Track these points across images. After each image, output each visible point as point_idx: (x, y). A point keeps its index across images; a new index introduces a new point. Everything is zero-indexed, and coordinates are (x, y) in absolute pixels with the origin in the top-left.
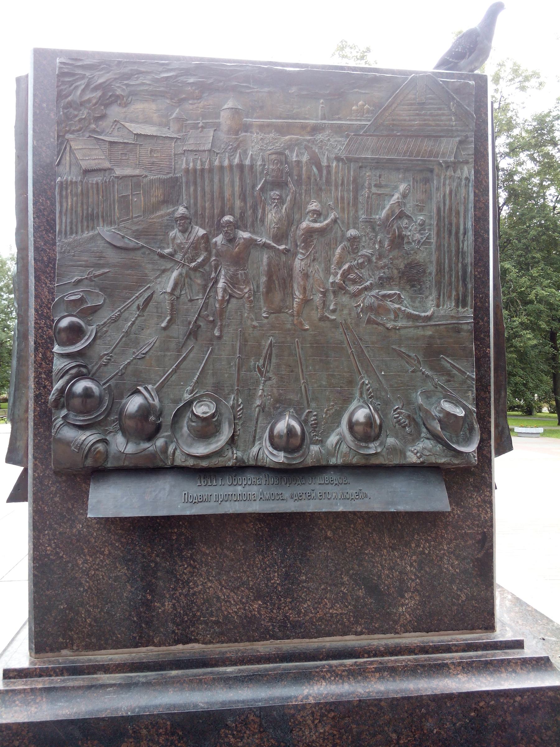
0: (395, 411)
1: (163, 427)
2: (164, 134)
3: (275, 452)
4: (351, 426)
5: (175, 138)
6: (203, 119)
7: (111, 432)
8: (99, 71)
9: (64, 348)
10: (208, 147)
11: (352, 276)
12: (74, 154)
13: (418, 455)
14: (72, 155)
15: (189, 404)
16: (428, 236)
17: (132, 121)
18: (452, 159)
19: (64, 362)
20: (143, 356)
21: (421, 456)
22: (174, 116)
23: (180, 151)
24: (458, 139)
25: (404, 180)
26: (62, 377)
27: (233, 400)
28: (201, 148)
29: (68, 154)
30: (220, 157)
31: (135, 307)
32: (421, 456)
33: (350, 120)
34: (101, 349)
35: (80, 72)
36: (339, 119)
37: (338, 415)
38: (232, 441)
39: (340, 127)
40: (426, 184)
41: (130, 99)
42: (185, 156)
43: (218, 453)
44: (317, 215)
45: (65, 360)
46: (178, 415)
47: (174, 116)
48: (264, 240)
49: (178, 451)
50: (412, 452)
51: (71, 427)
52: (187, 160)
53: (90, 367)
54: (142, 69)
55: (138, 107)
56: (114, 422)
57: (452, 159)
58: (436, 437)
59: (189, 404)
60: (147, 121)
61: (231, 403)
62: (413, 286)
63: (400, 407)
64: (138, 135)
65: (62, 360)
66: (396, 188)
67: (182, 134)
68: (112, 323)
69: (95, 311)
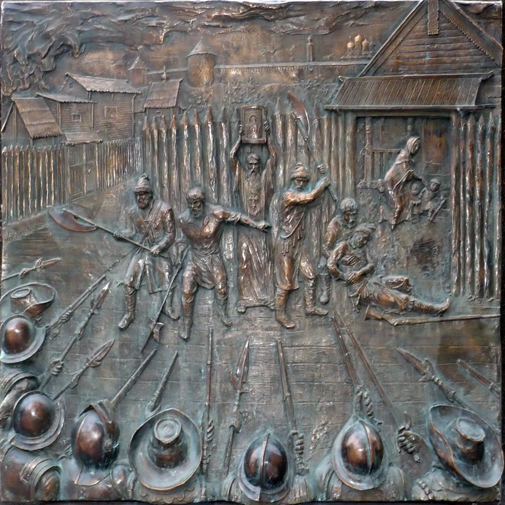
0: (401, 431)
1: (121, 452)
2: (123, 89)
3: (251, 487)
4: (346, 451)
5: (134, 94)
6: (167, 68)
7: (62, 458)
8: (48, 16)
9: (11, 357)
10: (173, 103)
11: (347, 258)
12: (21, 118)
13: (427, 490)
14: (19, 120)
15: (151, 423)
16: (444, 204)
17: (85, 74)
18: (473, 105)
19: (10, 374)
20: (99, 363)
21: (430, 492)
22: (132, 67)
23: (139, 109)
24: (480, 79)
25: (414, 133)
26: (9, 391)
27: (203, 419)
28: (166, 105)
29: (15, 119)
30: (187, 114)
31: (88, 303)
32: (430, 492)
33: (345, 60)
34: (54, 357)
35: (27, 19)
36: (331, 59)
37: (331, 435)
38: (202, 472)
39: (332, 69)
40: (441, 136)
41: (83, 48)
42: (146, 115)
43: (187, 486)
44: (304, 181)
45: (12, 370)
46: (138, 437)
47: (132, 67)
48: (238, 216)
49: (138, 483)
50: (420, 485)
51: (22, 452)
52: (148, 119)
53: (39, 377)
54: (97, 12)
55: (91, 58)
56: (67, 445)
57: (473, 105)
58: (448, 469)
59: (151, 423)
60: (105, 74)
61: (200, 422)
62: (425, 269)
63: (407, 426)
64: (92, 92)
65: (9, 370)
66: (403, 144)
67: (142, 89)
68: (64, 323)
69: (46, 308)
